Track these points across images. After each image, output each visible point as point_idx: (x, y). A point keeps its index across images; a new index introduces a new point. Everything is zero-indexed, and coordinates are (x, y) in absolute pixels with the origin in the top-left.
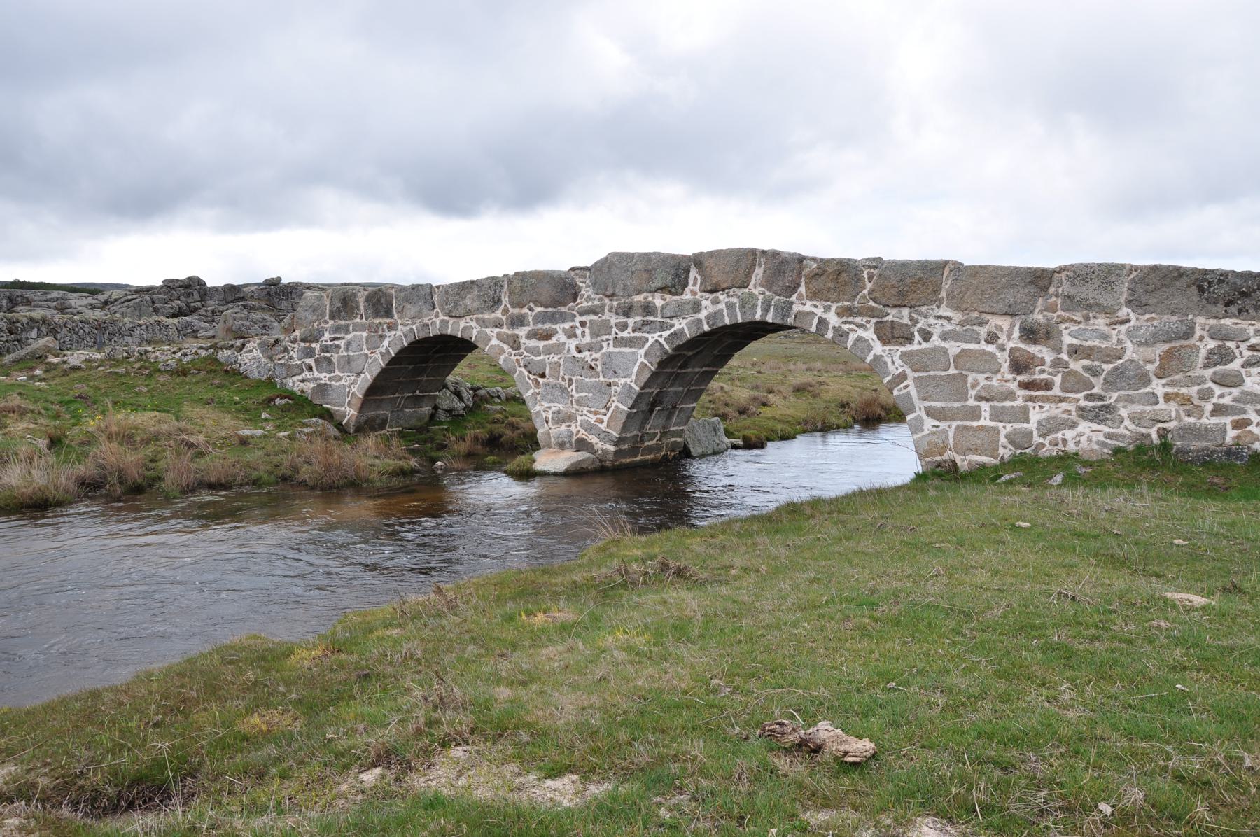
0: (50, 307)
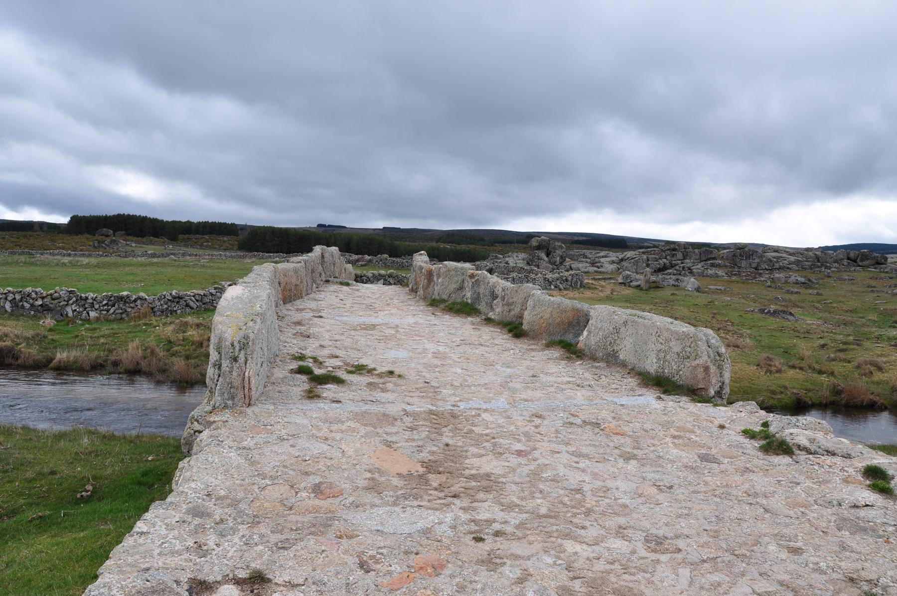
0: (587, 262)
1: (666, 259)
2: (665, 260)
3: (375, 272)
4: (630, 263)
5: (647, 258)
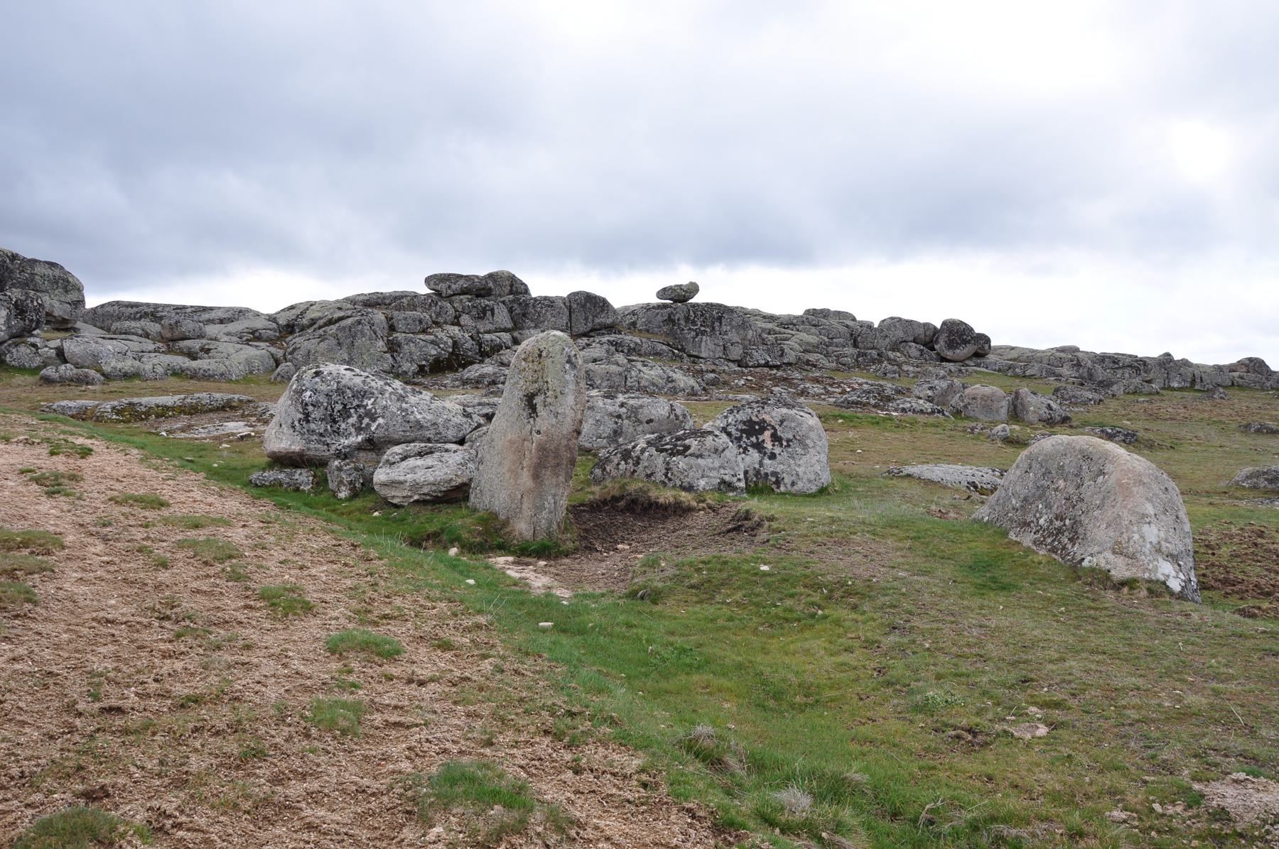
0: (147, 335)
1: (458, 324)
2: (455, 330)
3: (116, 403)
4: (322, 338)
5: (389, 319)
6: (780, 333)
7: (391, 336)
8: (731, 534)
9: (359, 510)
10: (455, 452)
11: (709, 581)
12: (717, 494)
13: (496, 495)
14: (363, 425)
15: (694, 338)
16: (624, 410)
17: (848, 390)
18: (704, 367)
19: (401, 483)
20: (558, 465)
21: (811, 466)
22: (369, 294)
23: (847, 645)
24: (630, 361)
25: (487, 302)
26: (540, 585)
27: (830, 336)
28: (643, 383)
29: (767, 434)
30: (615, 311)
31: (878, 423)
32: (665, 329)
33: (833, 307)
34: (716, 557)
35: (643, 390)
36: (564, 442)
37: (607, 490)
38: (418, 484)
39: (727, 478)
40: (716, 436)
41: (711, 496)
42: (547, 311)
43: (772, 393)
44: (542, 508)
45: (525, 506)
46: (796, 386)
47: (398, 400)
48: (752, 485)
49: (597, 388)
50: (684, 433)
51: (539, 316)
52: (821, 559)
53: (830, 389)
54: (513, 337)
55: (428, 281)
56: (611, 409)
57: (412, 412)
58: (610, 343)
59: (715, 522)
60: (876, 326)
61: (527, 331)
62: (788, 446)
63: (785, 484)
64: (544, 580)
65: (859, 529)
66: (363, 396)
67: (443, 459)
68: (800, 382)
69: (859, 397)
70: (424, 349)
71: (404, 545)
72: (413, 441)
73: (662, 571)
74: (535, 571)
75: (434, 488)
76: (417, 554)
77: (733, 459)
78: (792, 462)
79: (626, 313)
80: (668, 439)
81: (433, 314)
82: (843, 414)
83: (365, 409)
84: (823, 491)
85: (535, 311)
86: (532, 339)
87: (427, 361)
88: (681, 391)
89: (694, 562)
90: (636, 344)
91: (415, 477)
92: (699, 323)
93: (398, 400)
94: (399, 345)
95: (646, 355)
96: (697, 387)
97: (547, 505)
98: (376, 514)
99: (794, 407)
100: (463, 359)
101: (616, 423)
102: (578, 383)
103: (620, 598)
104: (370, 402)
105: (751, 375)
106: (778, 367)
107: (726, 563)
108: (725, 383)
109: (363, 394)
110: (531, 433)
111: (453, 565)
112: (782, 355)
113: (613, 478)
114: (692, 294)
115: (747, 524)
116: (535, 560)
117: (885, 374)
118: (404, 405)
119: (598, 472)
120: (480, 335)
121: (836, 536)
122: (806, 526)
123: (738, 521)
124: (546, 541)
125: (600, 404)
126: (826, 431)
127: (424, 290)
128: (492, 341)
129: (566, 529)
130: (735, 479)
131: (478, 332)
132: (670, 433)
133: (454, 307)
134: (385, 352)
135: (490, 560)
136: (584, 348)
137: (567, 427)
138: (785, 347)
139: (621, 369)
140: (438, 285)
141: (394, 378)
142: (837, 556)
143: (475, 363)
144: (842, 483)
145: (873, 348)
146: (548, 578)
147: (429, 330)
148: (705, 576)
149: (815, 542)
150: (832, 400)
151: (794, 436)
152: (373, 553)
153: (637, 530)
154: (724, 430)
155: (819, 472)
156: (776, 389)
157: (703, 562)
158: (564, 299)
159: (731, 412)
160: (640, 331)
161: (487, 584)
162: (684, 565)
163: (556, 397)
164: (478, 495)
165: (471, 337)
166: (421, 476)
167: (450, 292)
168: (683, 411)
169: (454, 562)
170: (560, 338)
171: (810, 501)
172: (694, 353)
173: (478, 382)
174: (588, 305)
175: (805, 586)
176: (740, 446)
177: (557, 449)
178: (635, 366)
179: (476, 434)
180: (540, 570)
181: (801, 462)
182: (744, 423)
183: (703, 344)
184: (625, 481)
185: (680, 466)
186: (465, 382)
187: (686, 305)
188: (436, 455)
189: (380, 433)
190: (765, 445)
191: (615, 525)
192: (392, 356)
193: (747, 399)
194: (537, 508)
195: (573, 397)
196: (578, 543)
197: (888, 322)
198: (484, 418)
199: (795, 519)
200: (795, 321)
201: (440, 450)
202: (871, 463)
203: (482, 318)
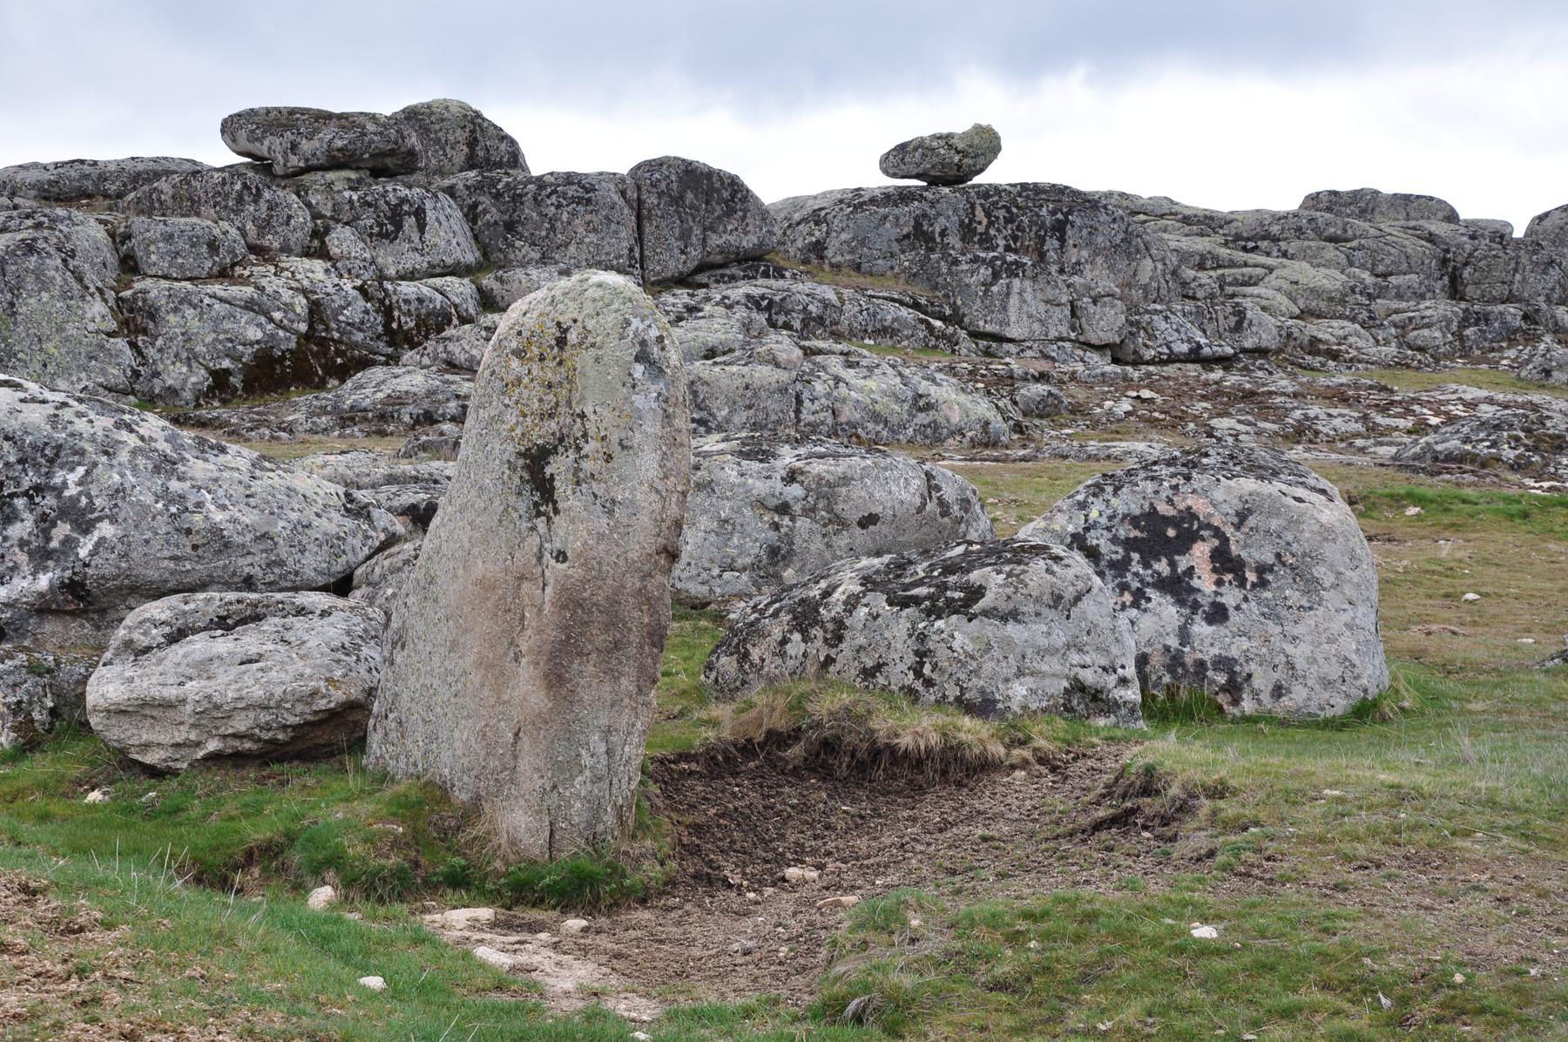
1: (323, 253)
5: (119, 238)
6: (1232, 264)
7: (128, 286)
8: (1104, 835)
9: (44, 787)
10: (325, 614)
11: (1047, 970)
12: (1061, 723)
13: (444, 735)
14: (54, 544)
15: (987, 285)
16: (796, 490)
17: (1434, 421)
18: (1016, 367)
19: (168, 705)
20: (617, 646)
21: (1330, 641)
22: (57, 165)
23: (851, 371)
24: (809, 353)
25: (404, 192)
26: (569, 985)
27: (1381, 268)
28: (847, 414)
29: (1200, 554)
30: (764, 214)
31: (1525, 516)
32: (905, 260)
33: (1389, 186)
34: (1065, 901)
35: (848, 434)
36: (633, 582)
37: (752, 714)
38: (217, 707)
39: (1088, 677)
40: (1057, 559)
41: (1044, 727)
42: (574, 214)
43: (1210, 435)
44: (574, 767)
45: (525, 764)
46: (1280, 414)
47: (157, 469)
48: (1161, 696)
49: (720, 428)
50: (967, 553)
51: (553, 228)
52: (1367, 907)
53: (1379, 419)
54: (480, 290)
55: (231, 128)
56: (760, 487)
57: (199, 505)
58: (754, 302)
59: (1058, 801)
60: (1519, 233)
61: (519, 273)
62: (1263, 584)
63: (1256, 694)
64: (582, 973)
65: (1478, 821)
66: (51, 461)
67: (289, 636)
68: (1291, 403)
69: (1466, 440)
70: (227, 325)
71: (179, 883)
72: (202, 586)
73: (913, 941)
74: (555, 946)
75: (264, 717)
76: (219, 909)
77: (1106, 623)
78: (1273, 629)
79: (797, 217)
80: (920, 569)
81: (249, 226)
82: (1420, 490)
83: (59, 496)
84: (1365, 712)
85: (540, 214)
86: (539, 294)
87: (237, 359)
88: (952, 434)
89: (1001, 915)
90: (826, 304)
91: (209, 687)
92: (1001, 242)
93: (157, 469)
94: (153, 313)
95: (852, 335)
96: (998, 423)
97: (586, 759)
98: (95, 796)
99: (1275, 474)
100: (339, 353)
101: (776, 527)
102: (668, 417)
103: (796, 1019)
104: (72, 478)
105: (1150, 387)
106: (1225, 362)
107: (1092, 917)
108: (1077, 410)
109: (53, 455)
110: (540, 558)
111: (322, 936)
112: (1238, 327)
113: (771, 680)
114: (981, 161)
115: (1150, 805)
116: (554, 914)
117: (1547, 373)
118: (175, 485)
119: (727, 663)
120: (388, 285)
121: (1409, 842)
122: (1318, 811)
123: (1124, 796)
124: (585, 863)
125: (731, 474)
126: (1370, 539)
127: (219, 155)
128: (420, 301)
129: (640, 826)
130: (1111, 680)
131: (381, 277)
132: (925, 553)
133: (309, 205)
134: (110, 335)
135: (428, 917)
136: (680, 319)
137: (642, 541)
138: (1247, 303)
139: (784, 376)
140: (260, 140)
141: (142, 407)
142: (1417, 898)
143: (373, 363)
144: (1421, 689)
145: (1510, 299)
146: (591, 966)
147: (238, 270)
148: (1033, 956)
149: (1348, 859)
150: (1387, 451)
151: (1278, 556)
152: (87, 909)
153: (841, 825)
154: (1078, 541)
155: (1354, 658)
156: (1222, 424)
157: (1028, 916)
158: (623, 179)
159: (1097, 490)
160: (836, 267)
161: (422, 989)
162: (972, 926)
163: (609, 458)
164: (393, 735)
165: (362, 289)
166: (225, 685)
167: (295, 161)
168: (962, 489)
169: (326, 928)
170: (616, 292)
171: (1329, 741)
172: (989, 328)
173: (382, 417)
174: (689, 196)
175: (1326, 986)
176: (1123, 587)
177: (613, 601)
178: (824, 368)
179: (383, 563)
180: (568, 944)
181: (1299, 630)
182: (1135, 521)
183: (1014, 301)
184: (804, 687)
185: (956, 645)
186: (347, 419)
187: (964, 192)
188: (271, 624)
189: (105, 566)
190: (1195, 583)
191: (778, 814)
192: (133, 345)
193: (1140, 456)
194: (558, 767)
195: (657, 456)
196: (674, 865)
197: (1556, 220)
198: (407, 519)
199: (1287, 792)
200: (1275, 229)
201: (282, 610)
202: (1510, 630)
203: (390, 237)
